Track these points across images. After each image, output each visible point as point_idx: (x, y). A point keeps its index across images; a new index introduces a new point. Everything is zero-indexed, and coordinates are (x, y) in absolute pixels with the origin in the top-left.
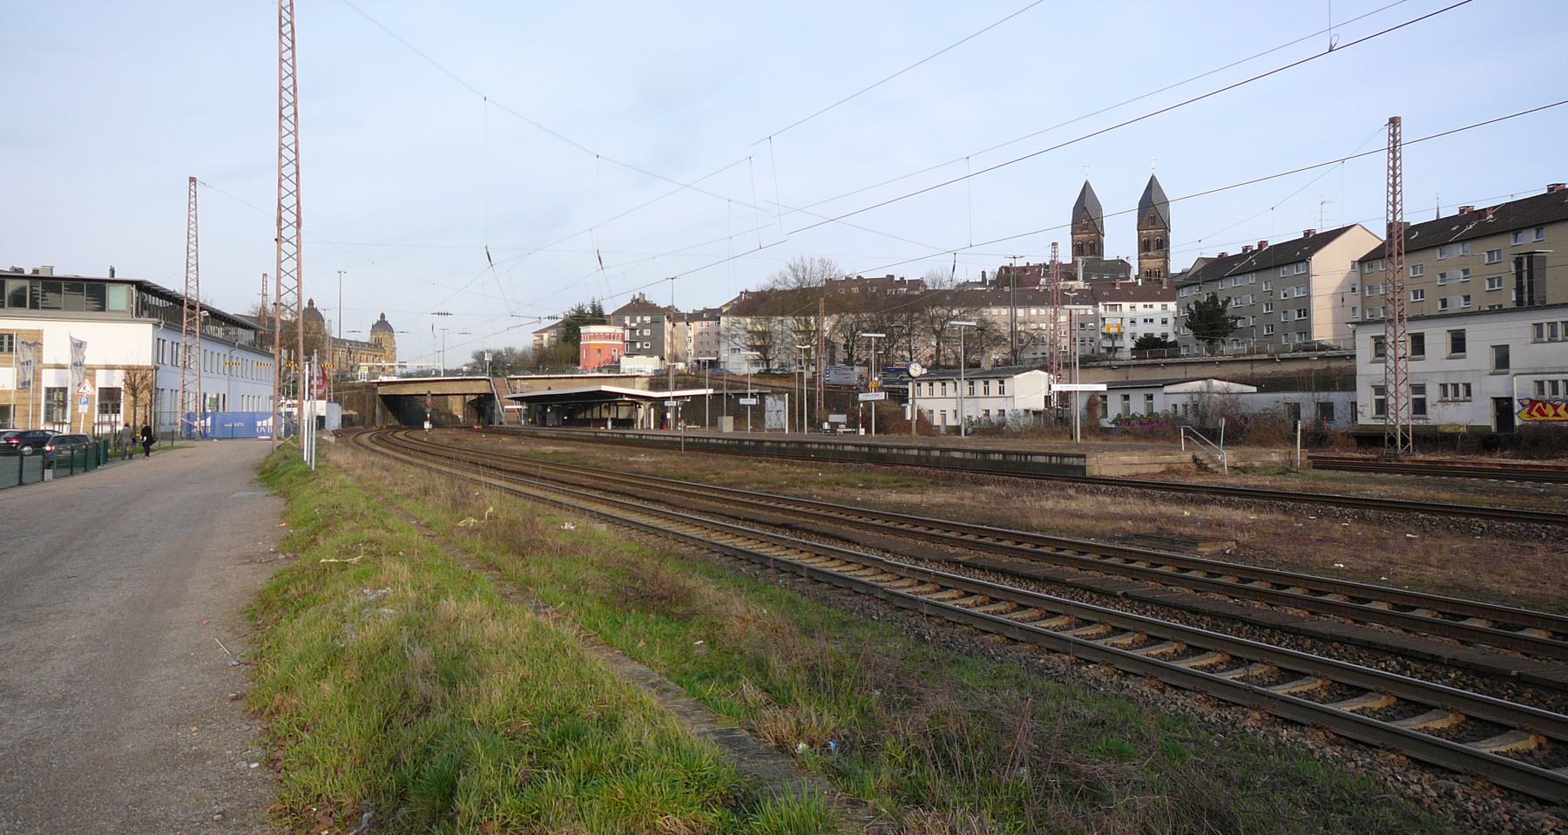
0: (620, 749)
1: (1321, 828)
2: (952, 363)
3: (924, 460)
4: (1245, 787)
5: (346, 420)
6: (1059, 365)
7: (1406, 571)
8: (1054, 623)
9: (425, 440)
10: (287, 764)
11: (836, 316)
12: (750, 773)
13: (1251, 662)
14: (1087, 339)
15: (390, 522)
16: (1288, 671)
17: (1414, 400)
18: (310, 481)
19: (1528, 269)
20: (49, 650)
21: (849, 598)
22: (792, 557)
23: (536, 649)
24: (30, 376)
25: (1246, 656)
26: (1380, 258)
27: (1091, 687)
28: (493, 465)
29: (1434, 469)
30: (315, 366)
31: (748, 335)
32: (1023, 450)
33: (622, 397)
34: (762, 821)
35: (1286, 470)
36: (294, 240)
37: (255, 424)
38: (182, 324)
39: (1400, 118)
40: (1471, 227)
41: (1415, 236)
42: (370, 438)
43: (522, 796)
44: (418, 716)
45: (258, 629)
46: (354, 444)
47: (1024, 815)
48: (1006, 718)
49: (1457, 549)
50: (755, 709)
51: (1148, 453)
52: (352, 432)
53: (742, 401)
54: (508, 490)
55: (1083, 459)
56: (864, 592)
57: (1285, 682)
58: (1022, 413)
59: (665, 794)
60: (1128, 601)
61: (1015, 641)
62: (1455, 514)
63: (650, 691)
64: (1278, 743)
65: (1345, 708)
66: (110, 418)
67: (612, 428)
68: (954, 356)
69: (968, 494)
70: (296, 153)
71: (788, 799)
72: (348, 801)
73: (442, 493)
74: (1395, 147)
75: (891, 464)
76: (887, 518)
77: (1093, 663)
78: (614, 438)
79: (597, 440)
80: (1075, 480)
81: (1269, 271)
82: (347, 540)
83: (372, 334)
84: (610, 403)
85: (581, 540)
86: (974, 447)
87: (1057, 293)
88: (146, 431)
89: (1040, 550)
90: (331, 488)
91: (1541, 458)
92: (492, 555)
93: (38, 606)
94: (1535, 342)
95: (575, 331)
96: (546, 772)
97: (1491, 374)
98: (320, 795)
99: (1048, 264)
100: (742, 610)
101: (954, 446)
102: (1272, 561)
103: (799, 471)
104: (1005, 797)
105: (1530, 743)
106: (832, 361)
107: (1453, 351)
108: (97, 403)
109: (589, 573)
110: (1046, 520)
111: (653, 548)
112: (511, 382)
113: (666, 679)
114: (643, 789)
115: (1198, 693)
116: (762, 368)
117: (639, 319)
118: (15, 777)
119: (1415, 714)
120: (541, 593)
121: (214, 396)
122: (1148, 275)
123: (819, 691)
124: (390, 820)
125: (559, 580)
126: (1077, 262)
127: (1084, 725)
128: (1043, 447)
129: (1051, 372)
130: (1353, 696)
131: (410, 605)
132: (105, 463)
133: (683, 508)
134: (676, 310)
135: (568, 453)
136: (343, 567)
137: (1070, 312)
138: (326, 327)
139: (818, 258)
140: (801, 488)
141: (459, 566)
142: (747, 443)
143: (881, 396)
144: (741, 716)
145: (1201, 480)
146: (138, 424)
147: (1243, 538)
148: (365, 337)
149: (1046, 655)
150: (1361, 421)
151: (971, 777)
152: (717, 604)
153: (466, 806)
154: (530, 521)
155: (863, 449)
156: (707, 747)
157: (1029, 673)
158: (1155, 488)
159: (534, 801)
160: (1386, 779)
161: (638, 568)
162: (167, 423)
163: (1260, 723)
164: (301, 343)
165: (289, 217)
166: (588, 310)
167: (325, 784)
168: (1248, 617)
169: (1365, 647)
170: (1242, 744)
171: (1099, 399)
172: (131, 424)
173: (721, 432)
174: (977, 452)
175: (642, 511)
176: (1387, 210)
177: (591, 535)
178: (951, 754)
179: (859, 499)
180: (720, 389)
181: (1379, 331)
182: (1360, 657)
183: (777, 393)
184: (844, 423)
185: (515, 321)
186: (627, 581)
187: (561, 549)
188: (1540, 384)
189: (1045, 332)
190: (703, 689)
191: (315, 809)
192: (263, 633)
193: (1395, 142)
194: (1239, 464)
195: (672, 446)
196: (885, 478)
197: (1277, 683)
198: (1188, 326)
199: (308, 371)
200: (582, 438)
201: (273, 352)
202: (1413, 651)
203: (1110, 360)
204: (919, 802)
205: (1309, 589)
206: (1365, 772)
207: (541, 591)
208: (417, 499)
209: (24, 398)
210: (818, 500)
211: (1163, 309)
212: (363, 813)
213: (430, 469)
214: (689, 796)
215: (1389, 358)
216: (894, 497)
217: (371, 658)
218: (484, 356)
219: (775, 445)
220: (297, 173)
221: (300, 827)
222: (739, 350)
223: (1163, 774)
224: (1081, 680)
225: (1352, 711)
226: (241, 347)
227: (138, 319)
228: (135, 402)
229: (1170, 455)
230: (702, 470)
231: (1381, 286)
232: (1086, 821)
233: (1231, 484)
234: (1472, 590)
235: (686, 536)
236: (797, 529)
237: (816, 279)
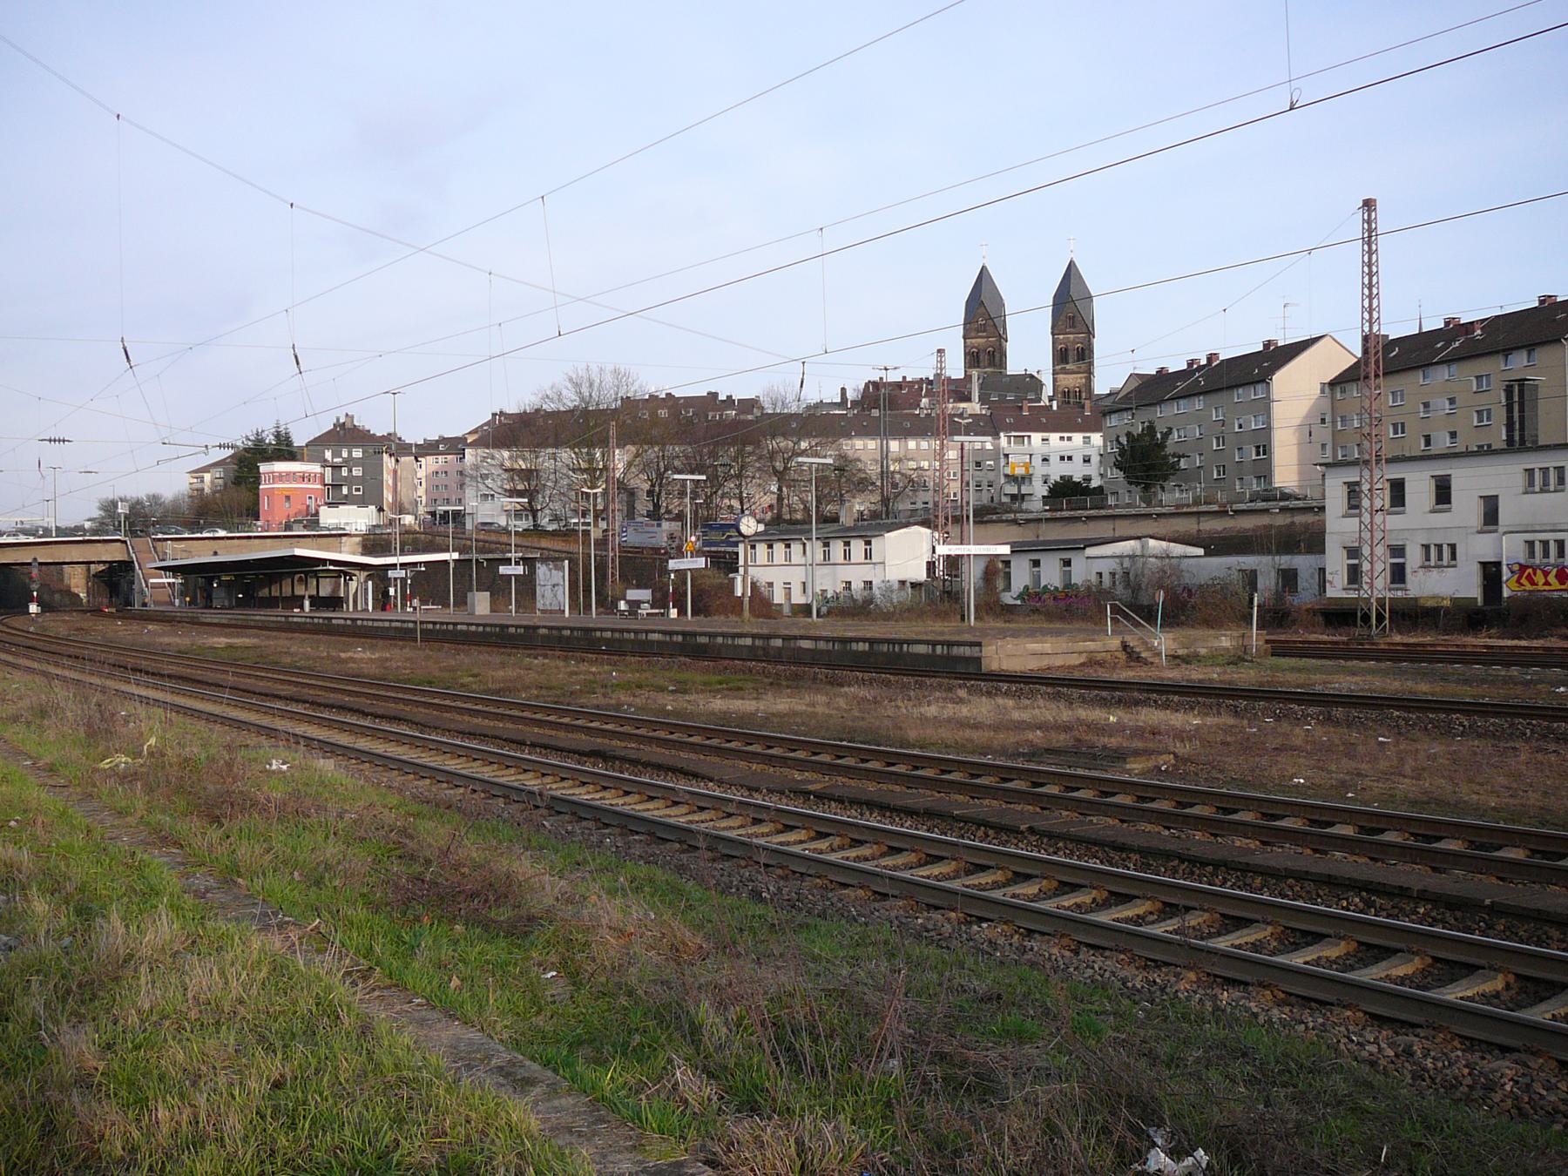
1: (1261, 1107)
2: (799, 516)
3: (760, 652)
4: (1173, 1066)
6: (946, 518)
7: (1376, 784)
8: (936, 870)
9: (32, 629)
11: (632, 449)
13: (1188, 909)
14: (985, 483)
16: (1233, 917)
17: (1393, 565)
19: (1519, 396)
25: (1183, 902)
26: (1353, 380)
27: (984, 952)
29: (1411, 654)
31: (505, 476)
32: (897, 636)
35: (1238, 658)
39: (1375, 200)
40: (1457, 344)
41: (1394, 353)
47: (893, 1119)
48: (871, 997)
49: (1435, 754)
51: (1064, 638)
53: (503, 570)
55: (977, 648)
57: (1228, 932)
58: (896, 586)
60: (1034, 838)
61: (885, 896)
62: (1434, 710)
64: (1216, 1008)
65: (1297, 960)
68: (802, 507)
69: (821, 698)
74: (1370, 237)
75: (714, 659)
76: (708, 733)
78: (313, 624)
80: (967, 676)
81: (1220, 394)
84: (306, 573)
86: (829, 634)
87: (944, 419)
89: (919, 772)
91: (1529, 638)
94: (1526, 493)
97: (1479, 532)
99: (931, 378)
101: (802, 632)
102: (1218, 779)
104: (868, 1097)
105: (1498, 984)
106: (631, 513)
107: (1438, 503)
110: (928, 732)
112: (159, 544)
115: (1120, 952)
119: (1377, 960)
125: (285, 862)
126: (971, 376)
127: (973, 1001)
130: (1308, 944)
134: (400, 439)
137: (962, 445)
139: (610, 368)
142: (512, 630)
143: (701, 562)
145: (1131, 673)
147: (1184, 749)
149: (925, 914)
150: (1331, 592)
151: (824, 1074)
155: (675, 638)
157: (902, 938)
158: (1072, 686)
160: (1339, 1041)
163: (1195, 986)
168: (1186, 852)
169: (1325, 882)
170: (1173, 1012)
171: (1000, 565)
173: (472, 614)
174: (834, 640)
175: (373, 733)
176: (1363, 318)
178: (797, 1046)
179: (669, 707)
180: (468, 553)
181: (1352, 475)
182: (1319, 896)
183: (553, 559)
184: (648, 602)
188: (1531, 544)
189: (927, 473)
193: (1370, 231)
194: (1180, 652)
195: (403, 635)
196: (706, 678)
197: (1219, 934)
198: (1118, 465)
202: (1379, 883)
203: (1015, 512)
204: (755, 1110)
205: (1261, 813)
206: (1316, 1035)
208: (28, 724)
210: (631, 713)
211: (1084, 443)
213: (44, 674)
215: (1363, 510)
216: (718, 704)
219: (554, 632)
222: (492, 496)
223: (1073, 1056)
224: (971, 943)
225: (1306, 963)
229: (1093, 640)
230: (451, 670)
231: (1355, 417)
232: (973, 1120)
233: (1169, 679)
234: (1449, 804)
236: (615, 758)
237: (608, 397)
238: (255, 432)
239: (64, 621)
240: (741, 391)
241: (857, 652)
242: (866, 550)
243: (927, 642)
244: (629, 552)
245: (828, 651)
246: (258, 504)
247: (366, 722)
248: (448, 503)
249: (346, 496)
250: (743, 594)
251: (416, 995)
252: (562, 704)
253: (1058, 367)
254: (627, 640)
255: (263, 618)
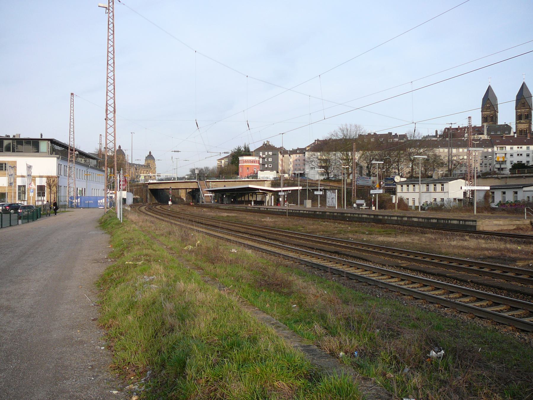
0: (258, 352)
3: (400, 222)
5: (135, 200)
6: (471, 177)
8: (437, 292)
9: (169, 209)
10: (116, 349)
11: (361, 152)
12: (318, 364)
14: (488, 164)
15: (154, 247)
18: (120, 227)
20: (24, 294)
21: (366, 287)
22: (339, 267)
23: (220, 306)
24: (12, 181)
28: (199, 222)
30: (121, 176)
31: (318, 161)
32: (447, 218)
33: (259, 190)
34: (322, 385)
36: (113, 119)
37: (97, 202)
38: (68, 158)
42: (145, 208)
43: (215, 369)
44: (169, 333)
45: (101, 291)
46: (138, 211)
50: (320, 336)
51: (508, 219)
52: (137, 206)
53: (316, 193)
54: (206, 233)
55: (475, 222)
56: (373, 284)
58: (452, 200)
59: (278, 372)
61: (417, 299)
63: (271, 327)
66: (41, 198)
67: (254, 205)
69: (417, 238)
70: (114, 80)
71: (335, 376)
72: (141, 366)
73: (177, 234)
75: (383, 224)
76: (375, 247)
77: (446, 307)
78: (255, 210)
79: (247, 211)
80: (469, 232)
82: (136, 254)
83: (145, 161)
84: (253, 193)
85: (240, 257)
88: (55, 204)
89: (433, 261)
90: (129, 230)
92: (199, 263)
93: (19, 276)
95: (236, 159)
96: (225, 360)
98: (129, 363)
100: (315, 291)
101: (414, 216)
103: (343, 226)
106: (361, 173)
108: (36, 192)
109: (243, 272)
111: (273, 261)
113: (279, 322)
114: (268, 369)
116: (325, 177)
117: (266, 153)
118: (16, 343)
120: (222, 281)
121: (81, 189)
122: (520, 132)
123: (350, 329)
124: (159, 375)
125: (230, 275)
126: (484, 126)
128: (455, 217)
129: (467, 180)
131: (164, 284)
132: (40, 218)
133: (287, 243)
134: (284, 149)
135: (233, 217)
136: (135, 266)
138: (126, 158)
140: (343, 234)
141: (185, 267)
142: (318, 213)
143: (381, 191)
144: (314, 340)
146: (52, 201)
148: (143, 162)
152: (303, 288)
153: (191, 372)
154: (216, 248)
156: (298, 352)
159: (220, 372)
161: (266, 271)
162: (63, 200)
164: (116, 166)
165: (111, 109)
166: (243, 149)
167: (131, 358)
168: (522, 291)
171: (490, 193)
172: (49, 201)
173: (305, 207)
177: (244, 255)
179: (365, 239)
180: (305, 187)
183: (332, 189)
185: (209, 155)
186: (261, 277)
187: (230, 261)
190: (296, 327)
191: (128, 368)
192: (103, 293)
195: (282, 214)
197: (527, 317)
199: (119, 178)
200: (240, 209)
201: (104, 169)
207: (221, 280)
208: (166, 236)
209: (11, 190)
211: (527, 149)
212: (147, 371)
213: (171, 223)
214: (289, 374)
216: (381, 239)
217: (148, 306)
218: (195, 171)
219: (332, 214)
220: (114, 89)
221: (122, 374)
222: (314, 168)
226: (91, 167)
227: (51, 156)
228: (51, 191)
230: (296, 225)
235: (288, 256)
236: (342, 254)
237: (353, 134)
238: (238, 147)
239: (179, 207)
240: (400, 132)
241: (433, 223)
242: (442, 187)
243: (457, 220)
244: (360, 187)
245: (423, 222)
246: (238, 170)
247: (266, 241)
248: (300, 170)
249: (267, 168)
250: (395, 202)
251: (256, 307)
252: (330, 237)
253: (518, 121)
254: (355, 217)
255: (239, 207)
